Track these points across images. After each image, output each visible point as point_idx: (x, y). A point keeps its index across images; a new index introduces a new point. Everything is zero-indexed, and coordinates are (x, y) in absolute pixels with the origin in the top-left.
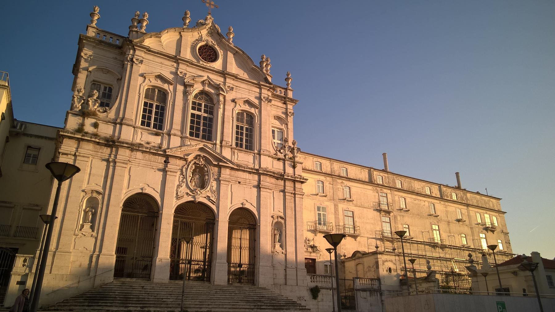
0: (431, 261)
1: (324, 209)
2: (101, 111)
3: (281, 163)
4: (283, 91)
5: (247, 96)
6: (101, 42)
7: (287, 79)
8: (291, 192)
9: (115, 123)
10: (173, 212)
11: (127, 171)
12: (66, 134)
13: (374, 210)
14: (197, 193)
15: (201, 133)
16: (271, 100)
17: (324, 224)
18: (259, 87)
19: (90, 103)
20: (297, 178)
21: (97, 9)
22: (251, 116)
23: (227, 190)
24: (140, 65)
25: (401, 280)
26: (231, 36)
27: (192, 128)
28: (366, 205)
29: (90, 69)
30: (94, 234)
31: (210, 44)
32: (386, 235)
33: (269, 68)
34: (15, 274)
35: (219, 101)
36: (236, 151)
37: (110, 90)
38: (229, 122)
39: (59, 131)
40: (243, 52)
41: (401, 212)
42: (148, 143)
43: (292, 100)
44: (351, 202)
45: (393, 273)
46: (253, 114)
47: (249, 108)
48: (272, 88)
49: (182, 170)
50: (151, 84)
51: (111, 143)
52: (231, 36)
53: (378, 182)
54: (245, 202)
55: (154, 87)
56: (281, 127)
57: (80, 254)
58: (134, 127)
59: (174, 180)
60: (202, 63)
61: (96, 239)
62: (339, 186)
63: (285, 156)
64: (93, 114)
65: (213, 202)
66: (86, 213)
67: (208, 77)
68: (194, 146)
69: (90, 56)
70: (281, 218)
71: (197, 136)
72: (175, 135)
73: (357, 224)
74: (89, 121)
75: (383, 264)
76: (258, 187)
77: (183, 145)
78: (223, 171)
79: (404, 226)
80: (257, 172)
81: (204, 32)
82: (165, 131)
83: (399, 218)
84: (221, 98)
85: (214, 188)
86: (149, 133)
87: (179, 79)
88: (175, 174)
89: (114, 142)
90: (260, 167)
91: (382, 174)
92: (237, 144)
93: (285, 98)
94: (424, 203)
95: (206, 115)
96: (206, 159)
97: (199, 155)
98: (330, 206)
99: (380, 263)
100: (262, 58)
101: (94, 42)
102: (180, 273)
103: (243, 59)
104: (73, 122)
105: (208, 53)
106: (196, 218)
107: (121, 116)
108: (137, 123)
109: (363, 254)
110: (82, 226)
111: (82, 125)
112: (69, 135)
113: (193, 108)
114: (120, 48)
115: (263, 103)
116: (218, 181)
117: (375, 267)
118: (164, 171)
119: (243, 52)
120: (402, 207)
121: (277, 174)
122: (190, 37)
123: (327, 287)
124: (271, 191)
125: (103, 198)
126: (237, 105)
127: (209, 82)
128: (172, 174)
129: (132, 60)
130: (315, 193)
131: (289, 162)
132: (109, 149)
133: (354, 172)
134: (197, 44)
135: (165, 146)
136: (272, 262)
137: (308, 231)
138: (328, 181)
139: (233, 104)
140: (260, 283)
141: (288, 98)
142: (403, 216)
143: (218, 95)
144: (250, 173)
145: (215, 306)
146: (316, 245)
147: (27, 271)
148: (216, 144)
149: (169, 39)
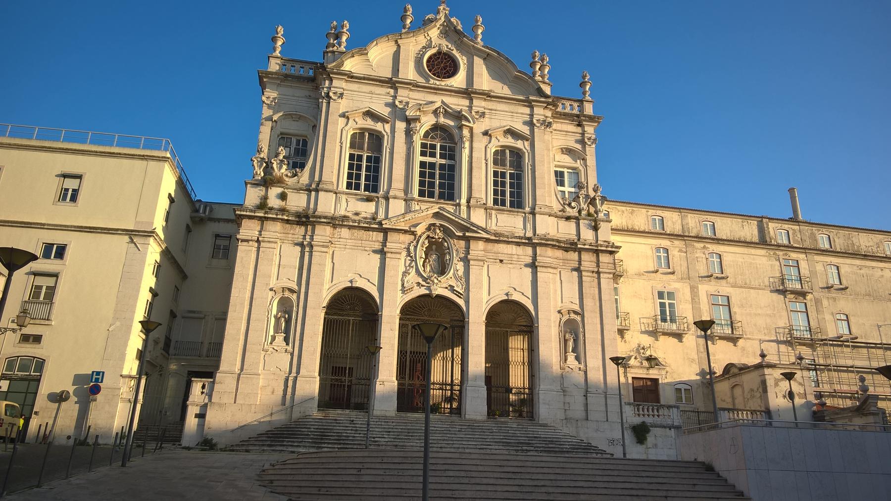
0: (868, 377)
1: (671, 295)
2: (289, 174)
3: (572, 225)
4: (576, 105)
5: (368, 105)
6: (286, 77)
7: (583, 84)
8: (592, 269)
9: (308, 190)
10: (398, 312)
11: (329, 256)
12: (245, 213)
13: (772, 291)
14: (433, 281)
15: (437, 190)
16: (550, 123)
17: (673, 321)
18: (530, 104)
19: (275, 166)
20: (601, 246)
21: (281, 30)
22: (517, 155)
23: (481, 274)
24: (340, 100)
25: (814, 413)
26: (480, 31)
27: (422, 184)
28: (755, 283)
29: (275, 118)
31: (445, 49)
32: (796, 334)
34: (193, 405)
35: (461, 137)
36: (494, 212)
37: (305, 143)
38: (480, 168)
39: (235, 210)
40: (498, 53)
41: (829, 292)
42: (357, 214)
43: (591, 119)
44: (724, 281)
45: (798, 401)
46: (520, 150)
47: (513, 141)
48: (551, 102)
49: (408, 249)
50: (358, 126)
51: (304, 219)
52: (480, 31)
53: (780, 242)
54: (512, 291)
55: (363, 131)
56: (575, 165)
57: (272, 377)
58: (336, 193)
59: (397, 265)
60: (435, 82)
61: (292, 354)
62: (699, 254)
63: (580, 212)
64: (279, 182)
65: (459, 294)
66: (277, 319)
67: (443, 102)
68: (425, 211)
69: (274, 99)
70: (575, 312)
71: (431, 195)
72: (395, 198)
73: (737, 317)
74: (274, 191)
75: (776, 385)
77: (408, 210)
78: (473, 244)
79: (838, 317)
80: (529, 242)
81: (434, 33)
82: (381, 192)
83: (825, 303)
84: (466, 132)
85: (461, 273)
86: (358, 200)
87: (399, 113)
88: (398, 256)
89: (307, 217)
90: (535, 235)
91: (786, 226)
92: (496, 202)
93: (578, 116)
94: (880, 273)
95: (443, 161)
96: (445, 230)
97: (434, 225)
98: (682, 290)
99: (770, 383)
100: (534, 57)
101: (278, 78)
102: (431, 403)
103: (499, 66)
104: (253, 196)
105: (443, 66)
106: (434, 323)
107: (317, 179)
108: (340, 186)
109: (741, 369)
110: (274, 338)
111: (265, 198)
112: (248, 213)
113: (423, 154)
114: (311, 80)
115: (536, 130)
116: (466, 261)
117: (761, 390)
118: (382, 252)
119: (498, 53)
120: (831, 282)
121: (564, 242)
122: (412, 45)
123: (665, 423)
124: (557, 271)
125: (298, 298)
126: (493, 139)
127: (446, 110)
128: (393, 256)
129: (328, 96)
130: (652, 269)
131: (586, 221)
132: (303, 228)
133: (726, 227)
134: (424, 53)
135: (381, 215)
136: (562, 384)
137: (642, 332)
138: (676, 248)
139: (487, 138)
140: (542, 417)
141: (585, 116)
142: (834, 299)
143: (460, 128)
144: (518, 244)
145: (452, 450)
146: (654, 355)
147: (206, 401)
148: (459, 205)
149: (380, 54)
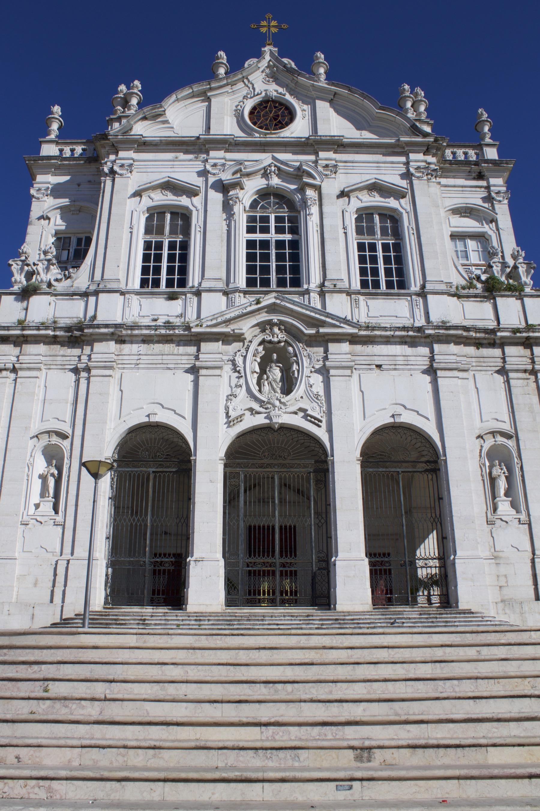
27: (250, 270)
30: (59, 518)
33: (422, 108)
35: (304, 201)
36: (361, 298)
38: (337, 239)
65: (316, 422)
66: (43, 478)
76: (431, 371)
84: (310, 193)
92: (364, 284)
96: (289, 330)
105: (271, 114)
116: (324, 372)
127: (279, 169)
143: (302, 190)
